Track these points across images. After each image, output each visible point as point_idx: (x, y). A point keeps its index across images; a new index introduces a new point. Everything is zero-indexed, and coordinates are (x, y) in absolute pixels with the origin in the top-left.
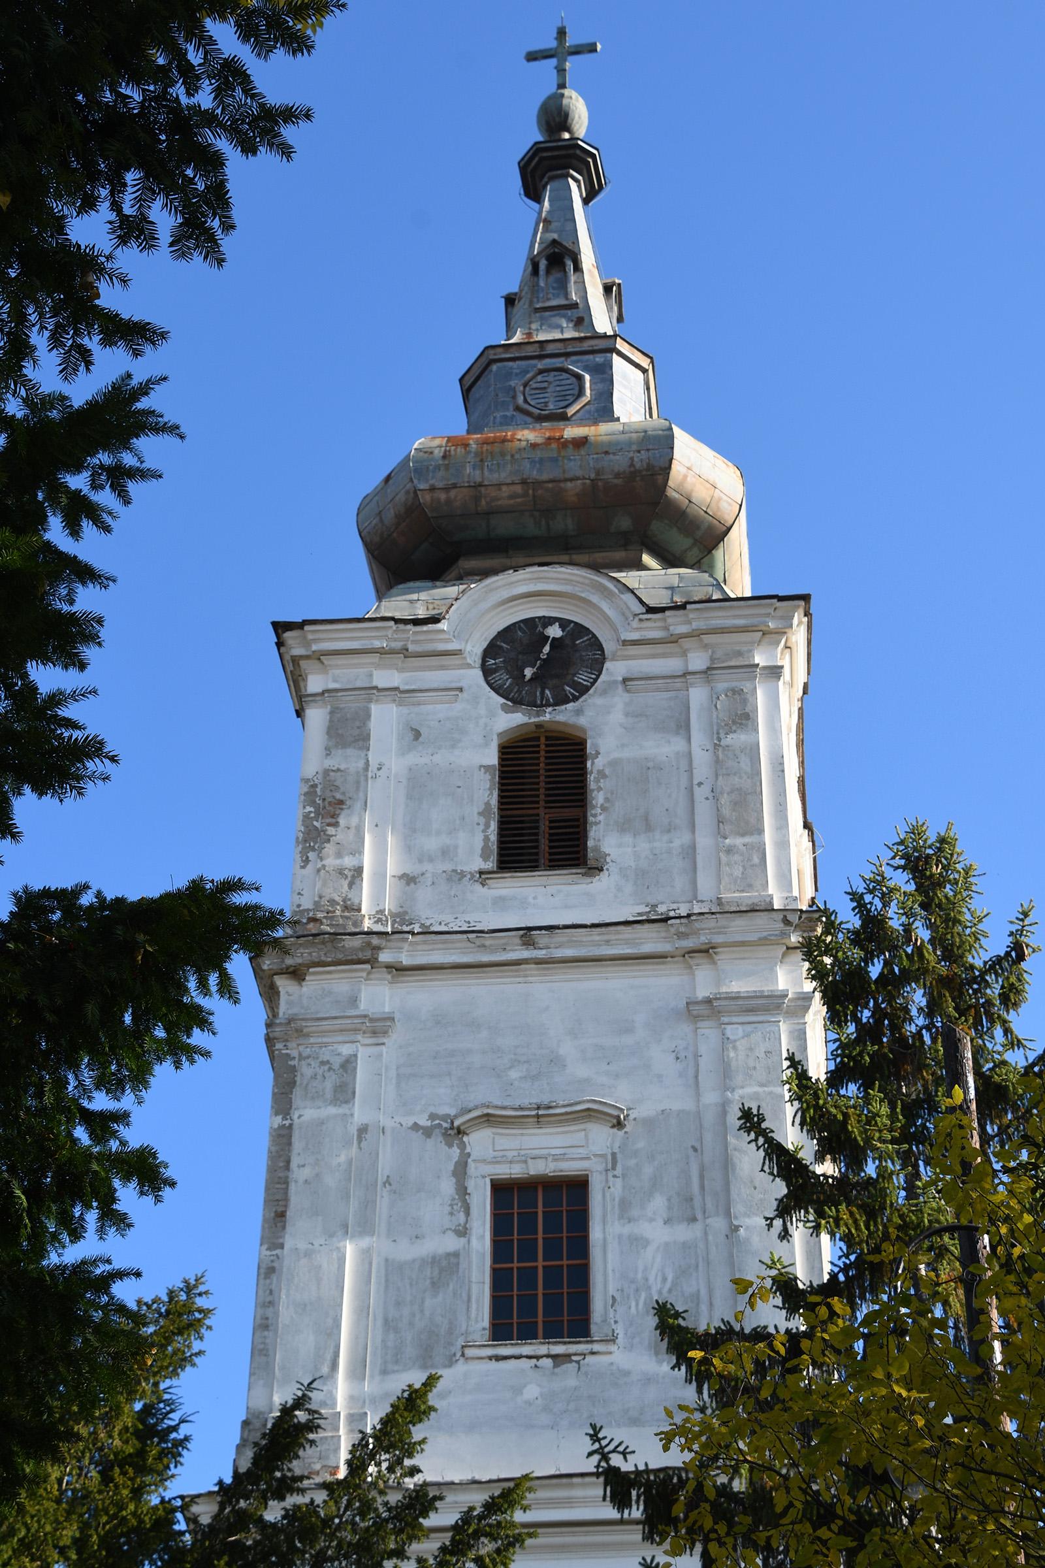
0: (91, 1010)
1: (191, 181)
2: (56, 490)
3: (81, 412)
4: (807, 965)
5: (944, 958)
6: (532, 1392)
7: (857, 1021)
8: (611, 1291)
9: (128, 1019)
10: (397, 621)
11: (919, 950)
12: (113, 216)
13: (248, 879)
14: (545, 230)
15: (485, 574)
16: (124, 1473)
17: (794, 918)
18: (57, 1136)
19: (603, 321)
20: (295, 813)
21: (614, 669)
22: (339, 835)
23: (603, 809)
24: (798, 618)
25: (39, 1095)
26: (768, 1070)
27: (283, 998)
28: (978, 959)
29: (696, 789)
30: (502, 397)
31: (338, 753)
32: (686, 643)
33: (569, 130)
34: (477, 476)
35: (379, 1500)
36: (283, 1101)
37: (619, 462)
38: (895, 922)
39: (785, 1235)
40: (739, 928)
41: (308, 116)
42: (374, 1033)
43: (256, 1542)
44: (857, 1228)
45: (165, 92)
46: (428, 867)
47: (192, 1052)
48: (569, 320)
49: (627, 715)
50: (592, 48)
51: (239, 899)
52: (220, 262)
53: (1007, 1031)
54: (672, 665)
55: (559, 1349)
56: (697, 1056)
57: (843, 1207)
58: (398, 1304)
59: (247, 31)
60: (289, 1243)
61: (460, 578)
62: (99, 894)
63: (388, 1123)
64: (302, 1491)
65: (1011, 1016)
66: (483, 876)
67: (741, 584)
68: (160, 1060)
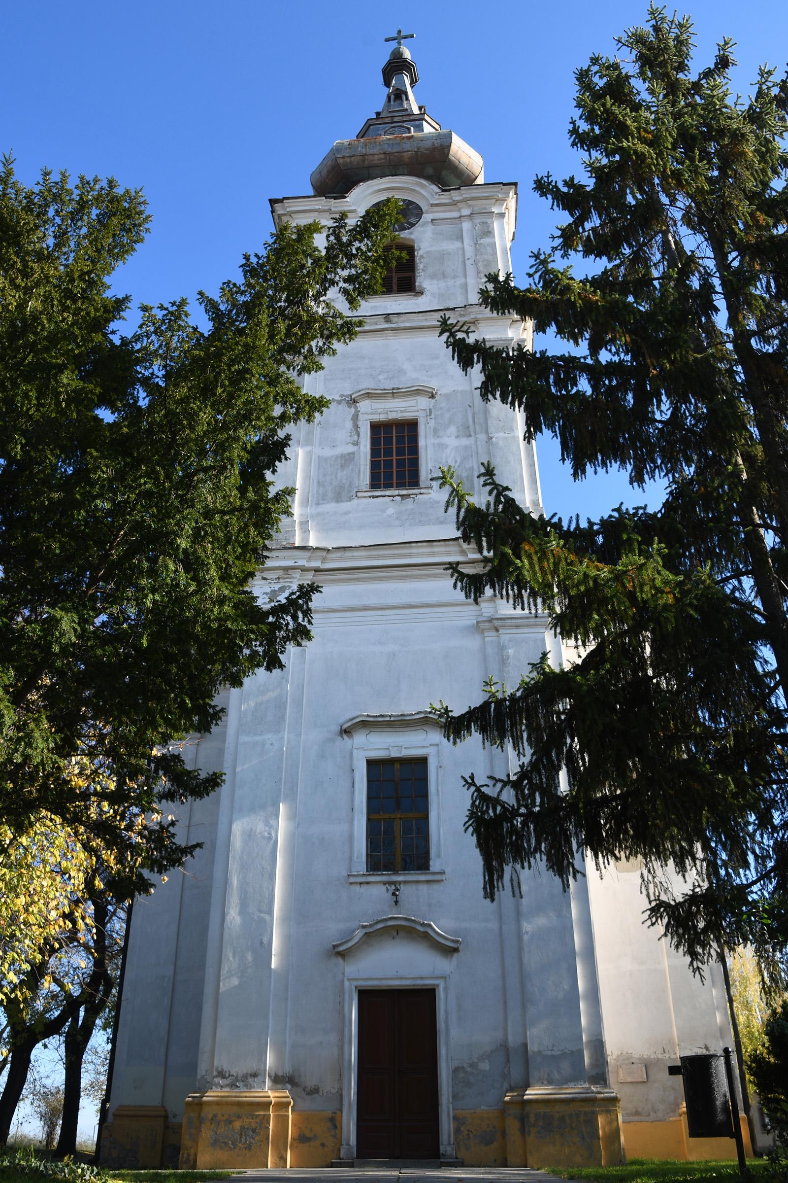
6: (391, 511)
8: (430, 467)
21: (427, 217)
23: (423, 270)
34: (364, 151)
37: (428, 144)
54: (455, 214)
58: (324, 475)
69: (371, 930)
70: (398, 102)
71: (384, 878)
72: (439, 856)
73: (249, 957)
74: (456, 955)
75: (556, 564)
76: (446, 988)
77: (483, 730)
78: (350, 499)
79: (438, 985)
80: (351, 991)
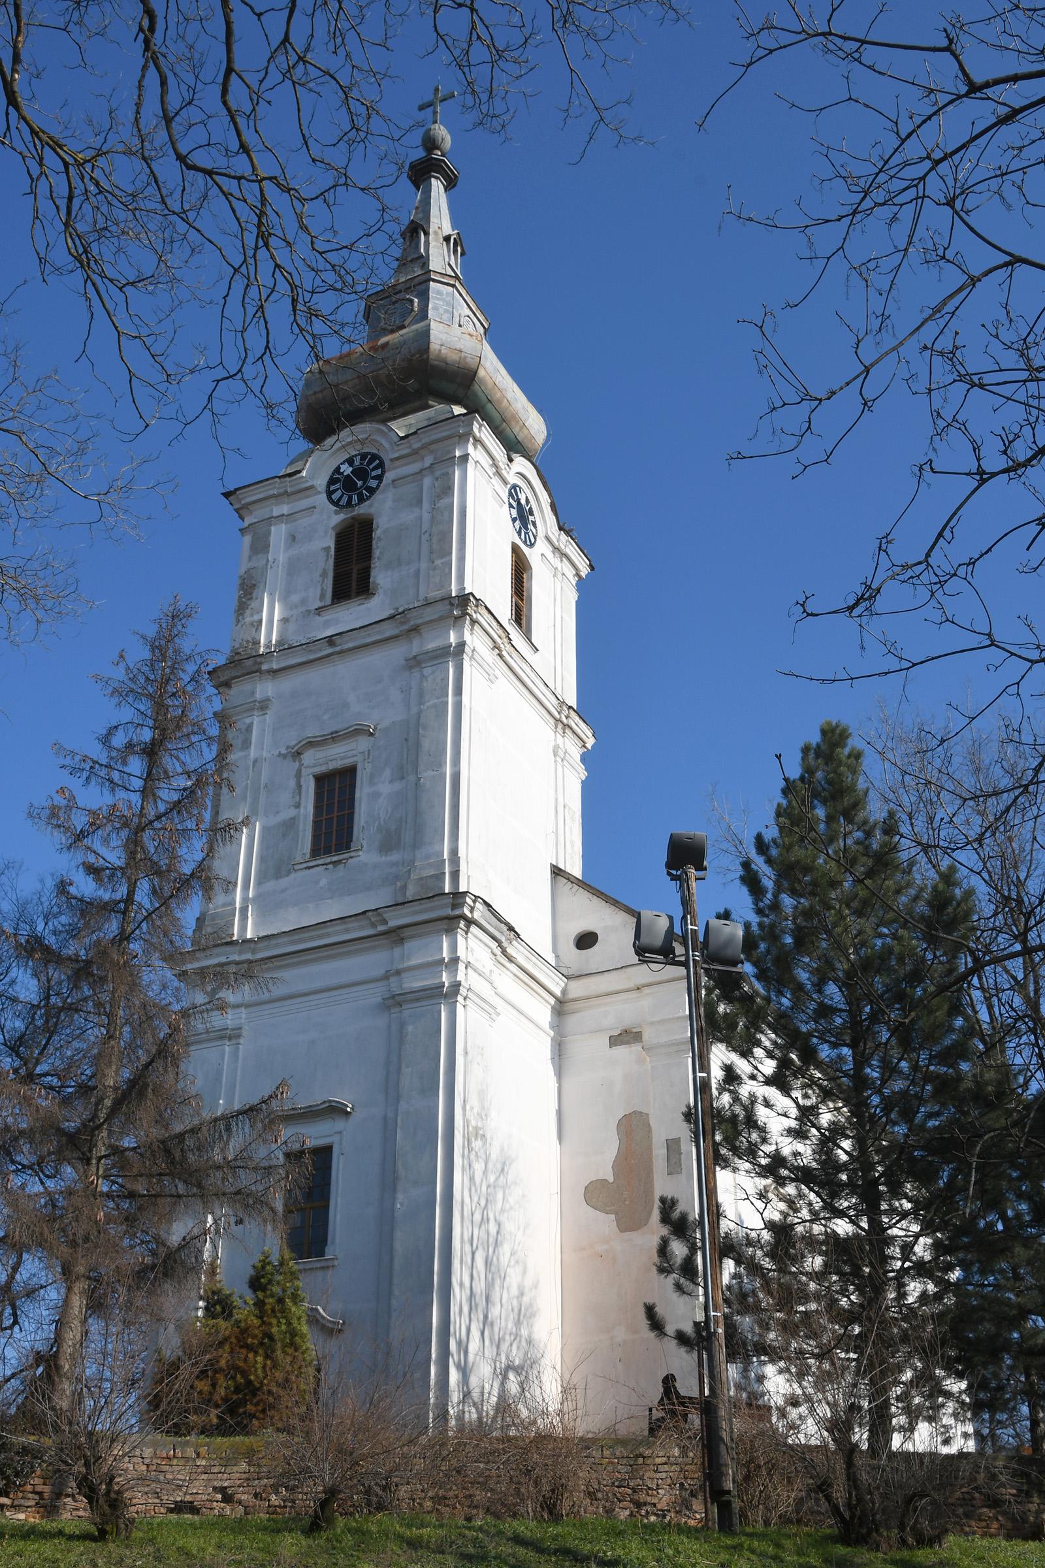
6: (323, 882)
8: (362, 824)
33: (438, 148)
40: (430, 614)
55: (335, 859)
66: (319, 611)
72: (333, 1243)
78: (288, 873)
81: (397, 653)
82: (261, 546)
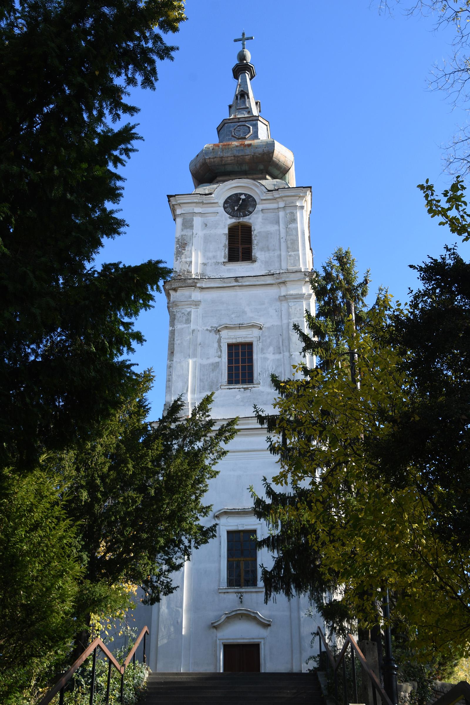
0: (123, 294)
1: (147, 67)
2: (111, 155)
3: (117, 133)
4: (311, 285)
5: (347, 283)
6: (238, 397)
7: (324, 300)
8: (259, 372)
9: (133, 298)
10: (200, 194)
11: (340, 281)
12: (126, 78)
13: (163, 260)
14: (240, 87)
15: (224, 181)
16: (135, 416)
17: (307, 274)
18: (115, 328)
19: (255, 112)
20: (174, 247)
21: (259, 207)
22: (185, 252)
23: (256, 245)
24: (308, 193)
25: (111, 317)
26: (300, 314)
27: (172, 296)
28: (355, 284)
29: (282, 240)
30: (228, 133)
31: (185, 230)
32: (278, 200)
33: (245, 60)
34: (222, 155)
35: (200, 423)
36: (172, 323)
37: (260, 150)
38: (334, 274)
39: (304, 356)
40: (293, 276)
41: (178, 49)
42: (196, 305)
43: (169, 433)
44: (323, 354)
45: (139, 43)
46: (209, 261)
47: (149, 306)
48: (246, 112)
49: (263, 219)
50: (252, 38)
51: (161, 265)
52: (154, 89)
53: (363, 302)
54: (274, 206)
55: (245, 386)
56: (281, 311)
57: (319, 349)
58: (203, 375)
59: (161, 27)
60: (175, 360)
61: (217, 183)
62: (124, 265)
63: (200, 329)
64: (180, 421)
65: (364, 299)
67: (293, 183)
68: (141, 309)
69: (229, 615)
70: (243, 99)
71: (236, 590)
73: (172, 629)
74: (269, 628)
75: (280, 515)
76: (264, 644)
77: (268, 546)
79: (261, 642)
80: (220, 645)
81: (273, 292)
82: (188, 224)
